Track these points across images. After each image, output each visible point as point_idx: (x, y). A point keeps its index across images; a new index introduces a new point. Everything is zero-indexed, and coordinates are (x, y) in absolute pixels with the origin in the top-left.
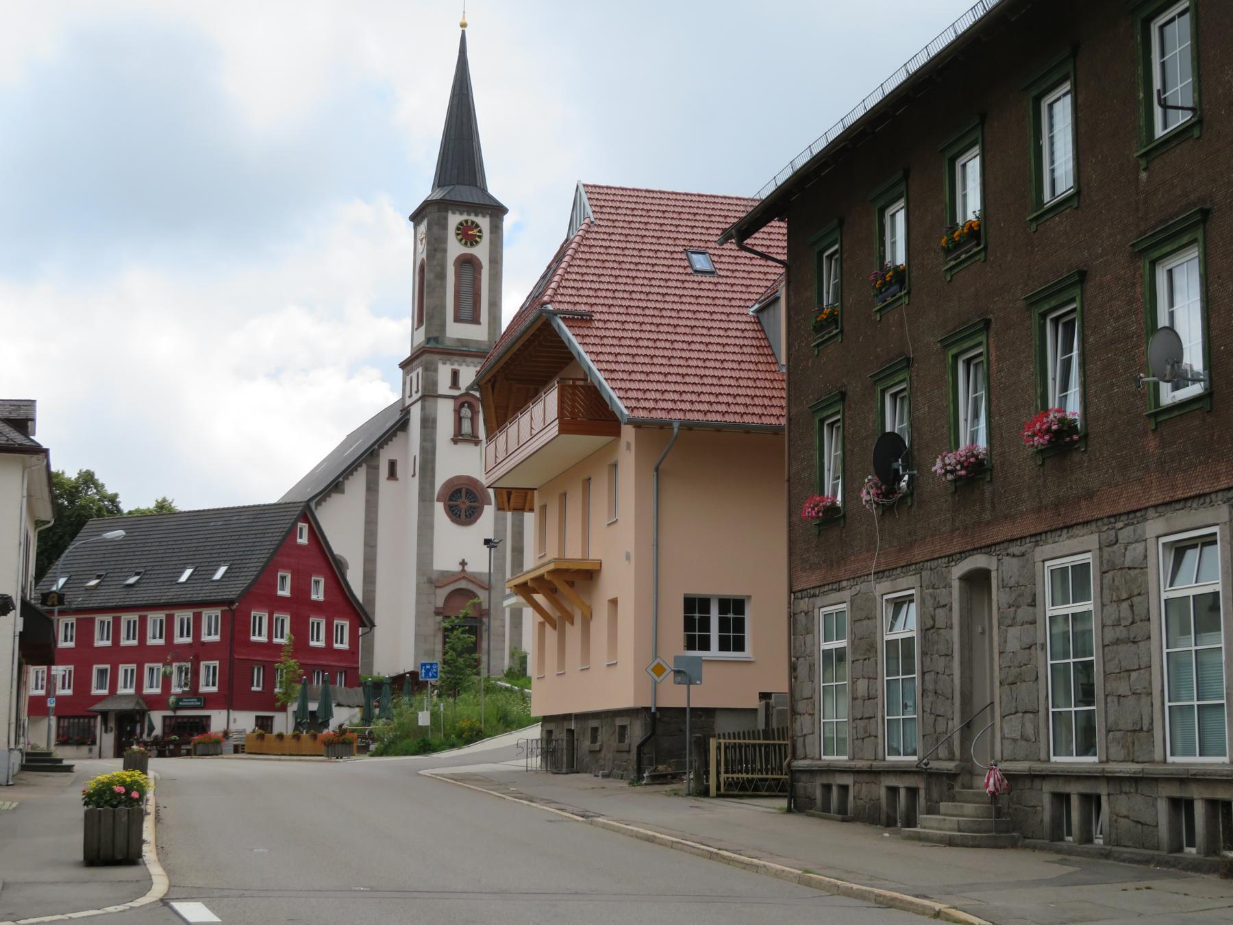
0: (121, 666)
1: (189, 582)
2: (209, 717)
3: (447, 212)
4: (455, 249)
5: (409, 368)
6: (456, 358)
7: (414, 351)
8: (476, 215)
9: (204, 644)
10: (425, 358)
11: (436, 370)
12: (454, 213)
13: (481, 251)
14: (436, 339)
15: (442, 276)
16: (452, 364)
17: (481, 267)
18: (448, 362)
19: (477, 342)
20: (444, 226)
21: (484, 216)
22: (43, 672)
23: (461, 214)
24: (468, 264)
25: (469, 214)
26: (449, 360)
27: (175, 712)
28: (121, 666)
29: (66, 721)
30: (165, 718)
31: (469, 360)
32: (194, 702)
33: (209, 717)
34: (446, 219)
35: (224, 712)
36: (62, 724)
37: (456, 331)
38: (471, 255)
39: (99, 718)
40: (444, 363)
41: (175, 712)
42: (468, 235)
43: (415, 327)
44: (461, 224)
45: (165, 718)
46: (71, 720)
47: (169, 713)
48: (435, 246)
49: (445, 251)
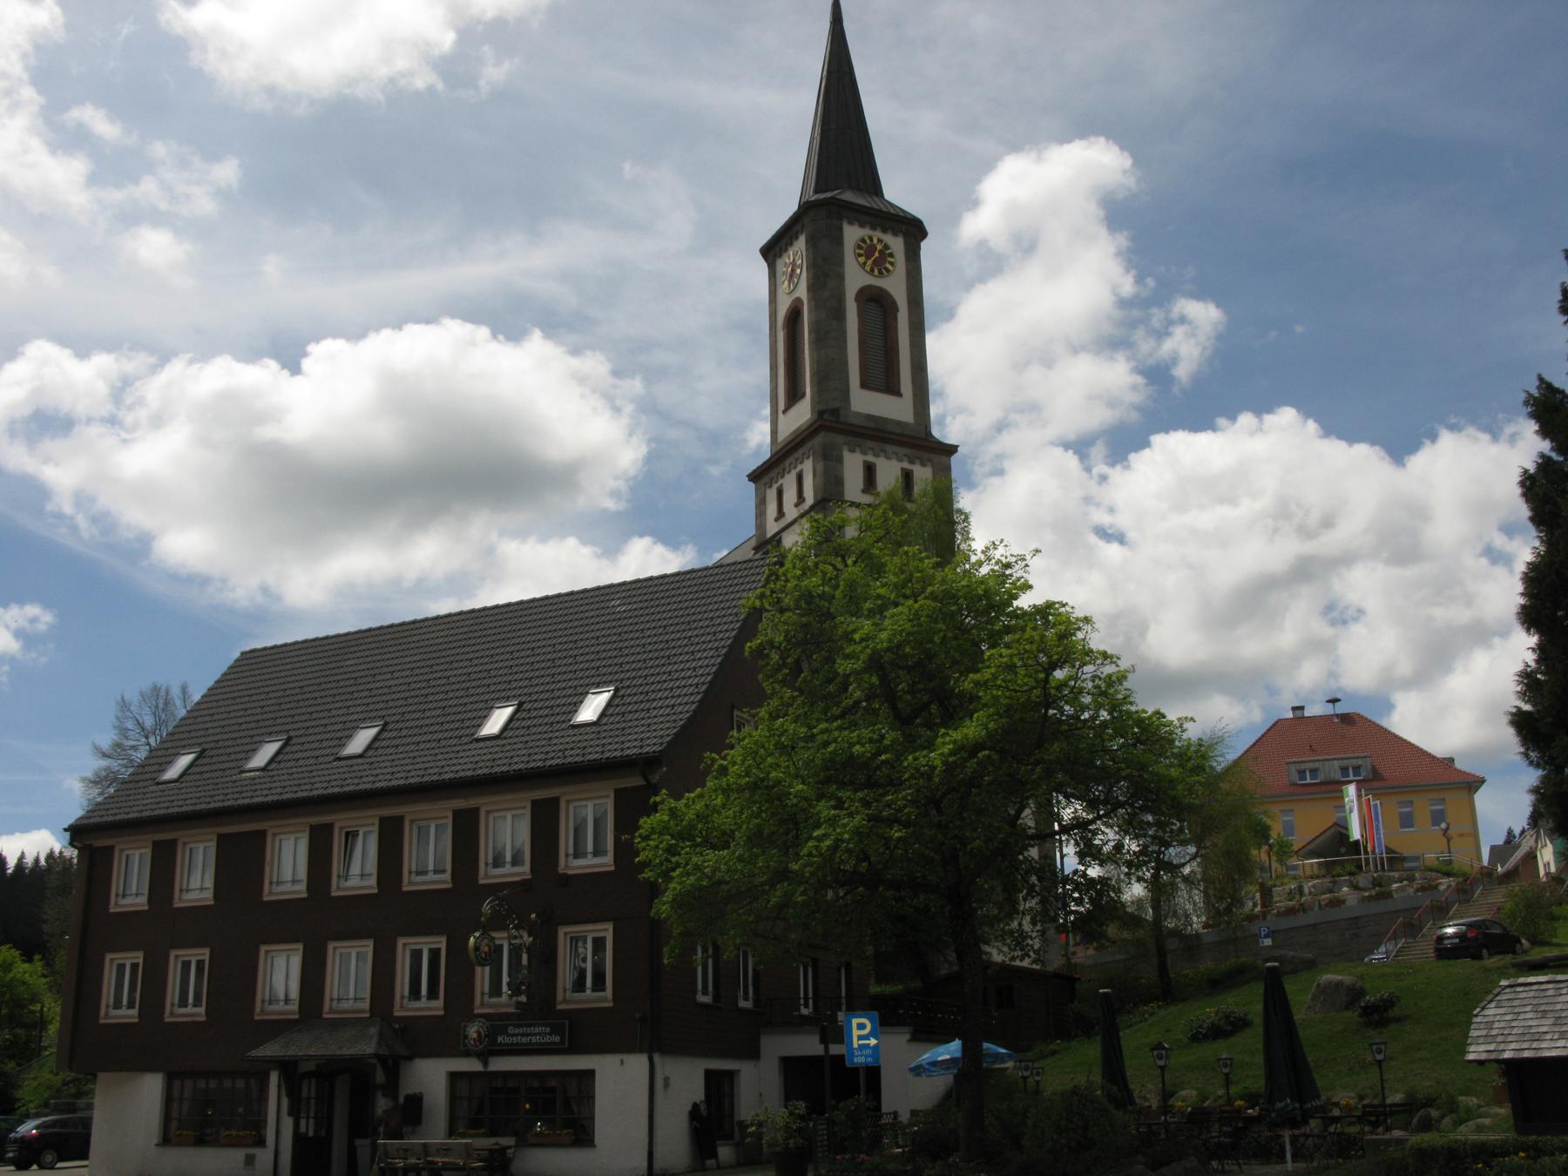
0: (401, 941)
1: (515, 724)
2: (591, 1074)
3: (842, 219)
4: (856, 277)
5: (766, 479)
6: (870, 444)
7: (777, 453)
8: (884, 231)
9: (567, 880)
10: (817, 441)
11: (840, 460)
12: (850, 223)
13: (895, 285)
14: (835, 412)
15: (839, 314)
16: (864, 453)
17: (897, 309)
18: (858, 449)
19: (899, 423)
20: (839, 241)
21: (895, 234)
22: (599, 944)
23: (862, 225)
24: (876, 303)
25: (873, 228)
26: (860, 446)
27: (486, 1063)
28: (401, 941)
29: (189, 1084)
30: (454, 1077)
31: (890, 448)
32: (540, 1034)
33: (591, 1074)
34: (840, 230)
35: (637, 1064)
36: (176, 1093)
37: (865, 403)
38: (881, 290)
39: (274, 1078)
40: (852, 451)
41: (486, 1063)
42: (878, 261)
43: (781, 405)
44: (863, 240)
45: (454, 1077)
46: (201, 1084)
47: (471, 1065)
48: (825, 273)
49: (841, 277)
